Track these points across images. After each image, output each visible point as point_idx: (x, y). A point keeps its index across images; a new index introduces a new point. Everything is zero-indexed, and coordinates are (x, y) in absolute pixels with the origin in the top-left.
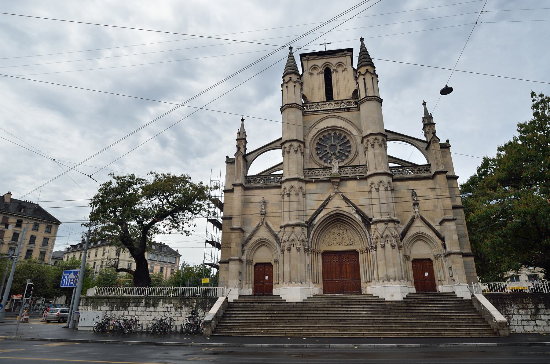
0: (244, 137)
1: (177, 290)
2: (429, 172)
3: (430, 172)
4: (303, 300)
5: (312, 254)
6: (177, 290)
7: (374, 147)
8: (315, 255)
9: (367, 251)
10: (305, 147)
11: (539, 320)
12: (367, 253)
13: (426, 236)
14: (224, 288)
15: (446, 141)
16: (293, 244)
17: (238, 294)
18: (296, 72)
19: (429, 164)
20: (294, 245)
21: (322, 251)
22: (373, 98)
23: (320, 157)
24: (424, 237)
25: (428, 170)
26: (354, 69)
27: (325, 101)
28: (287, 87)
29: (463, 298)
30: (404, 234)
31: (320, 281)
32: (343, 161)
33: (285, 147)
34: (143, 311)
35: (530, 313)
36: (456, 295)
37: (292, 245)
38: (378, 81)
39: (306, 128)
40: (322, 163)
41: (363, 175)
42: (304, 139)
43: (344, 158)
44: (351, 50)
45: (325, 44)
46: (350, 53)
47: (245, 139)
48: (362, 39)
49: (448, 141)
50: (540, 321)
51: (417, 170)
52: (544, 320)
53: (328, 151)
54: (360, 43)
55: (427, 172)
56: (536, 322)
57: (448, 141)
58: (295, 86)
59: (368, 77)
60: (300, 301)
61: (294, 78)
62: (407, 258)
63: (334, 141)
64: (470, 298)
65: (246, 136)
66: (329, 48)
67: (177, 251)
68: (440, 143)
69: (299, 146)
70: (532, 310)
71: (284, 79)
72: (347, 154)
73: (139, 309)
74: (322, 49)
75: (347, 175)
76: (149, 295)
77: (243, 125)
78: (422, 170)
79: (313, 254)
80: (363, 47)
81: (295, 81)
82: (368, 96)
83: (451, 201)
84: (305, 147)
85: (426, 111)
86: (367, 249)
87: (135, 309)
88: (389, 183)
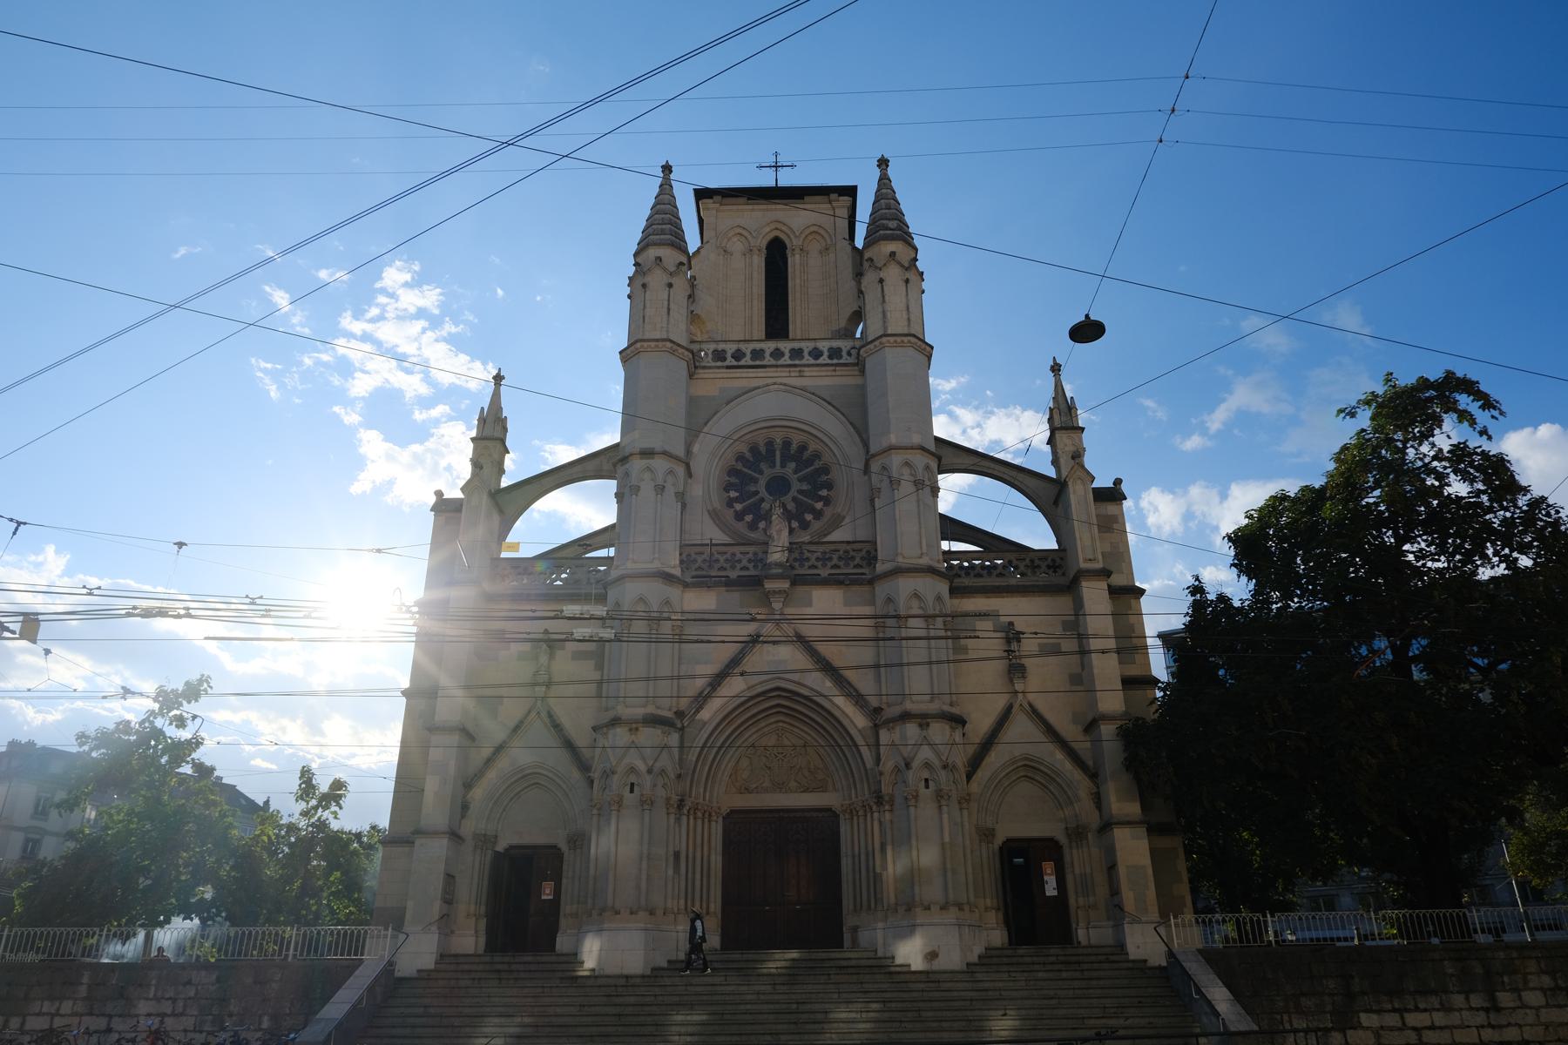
0: (498, 434)
1: (249, 939)
2: (1060, 572)
3: (1064, 574)
4: (967, 964)
5: (691, 817)
6: (249, 939)
7: (664, 494)
8: (699, 822)
9: (865, 811)
10: (689, 474)
11: (1355, 1028)
12: (866, 816)
13: (1042, 768)
14: (387, 929)
15: (1114, 484)
16: (632, 785)
17: (434, 949)
18: (678, 242)
19: (1062, 548)
20: (636, 788)
21: (725, 811)
22: (906, 339)
23: (736, 512)
24: (1038, 770)
25: (1058, 567)
26: (855, 248)
27: (764, 337)
28: (644, 286)
29: (1145, 961)
30: (975, 763)
31: (712, 906)
32: (805, 526)
33: (627, 474)
34: (82, 1015)
35: (1329, 1008)
36: (1127, 954)
37: (628, 788)
38: (923, 292)
39: (697, 417)
40: (741, 527)
41: (819, 575)
42: (688, 452)
43: (809, 517)
44: (851, 192)
45: (776, 167)
46: (847, 200)
47: (503, 441)
48: (883, 163)
49: (1118, 482)
50: (1360, 1032)
51: (1026, 566)
52: (1368, 1028)
53: (796, 494)
54: (877, 173)
55: (1055, 572)
56: (1345, 1036)
57: (1118, 482)
58: (907, 281)
59: (893, 274)
60: (957, 968)
61: (670, 256)
62: (987, 834)
63: (781, 463)
64: (1164, 964)
65: (505, 430)
66: (787, 179)
67: (267, 803)
68: (1093, 488)
69: (671, 472)
70: (1335, 998)
71: (639, 260)
72: (738, 507)
73: (67, 1007)
74: (766, 180)
75: (815, 572)
76: (301, 955)
77: (496, 396)
78: (1039, 567)
79: (695, 818)
80: (884, 181)
81: (672, 270)
82: (889, 332)
83: (1120, 663)
84: (689, 474)
85: (1059, 389)
86: (864, 806)
87: (47, 1007)
88: (939, 598)
